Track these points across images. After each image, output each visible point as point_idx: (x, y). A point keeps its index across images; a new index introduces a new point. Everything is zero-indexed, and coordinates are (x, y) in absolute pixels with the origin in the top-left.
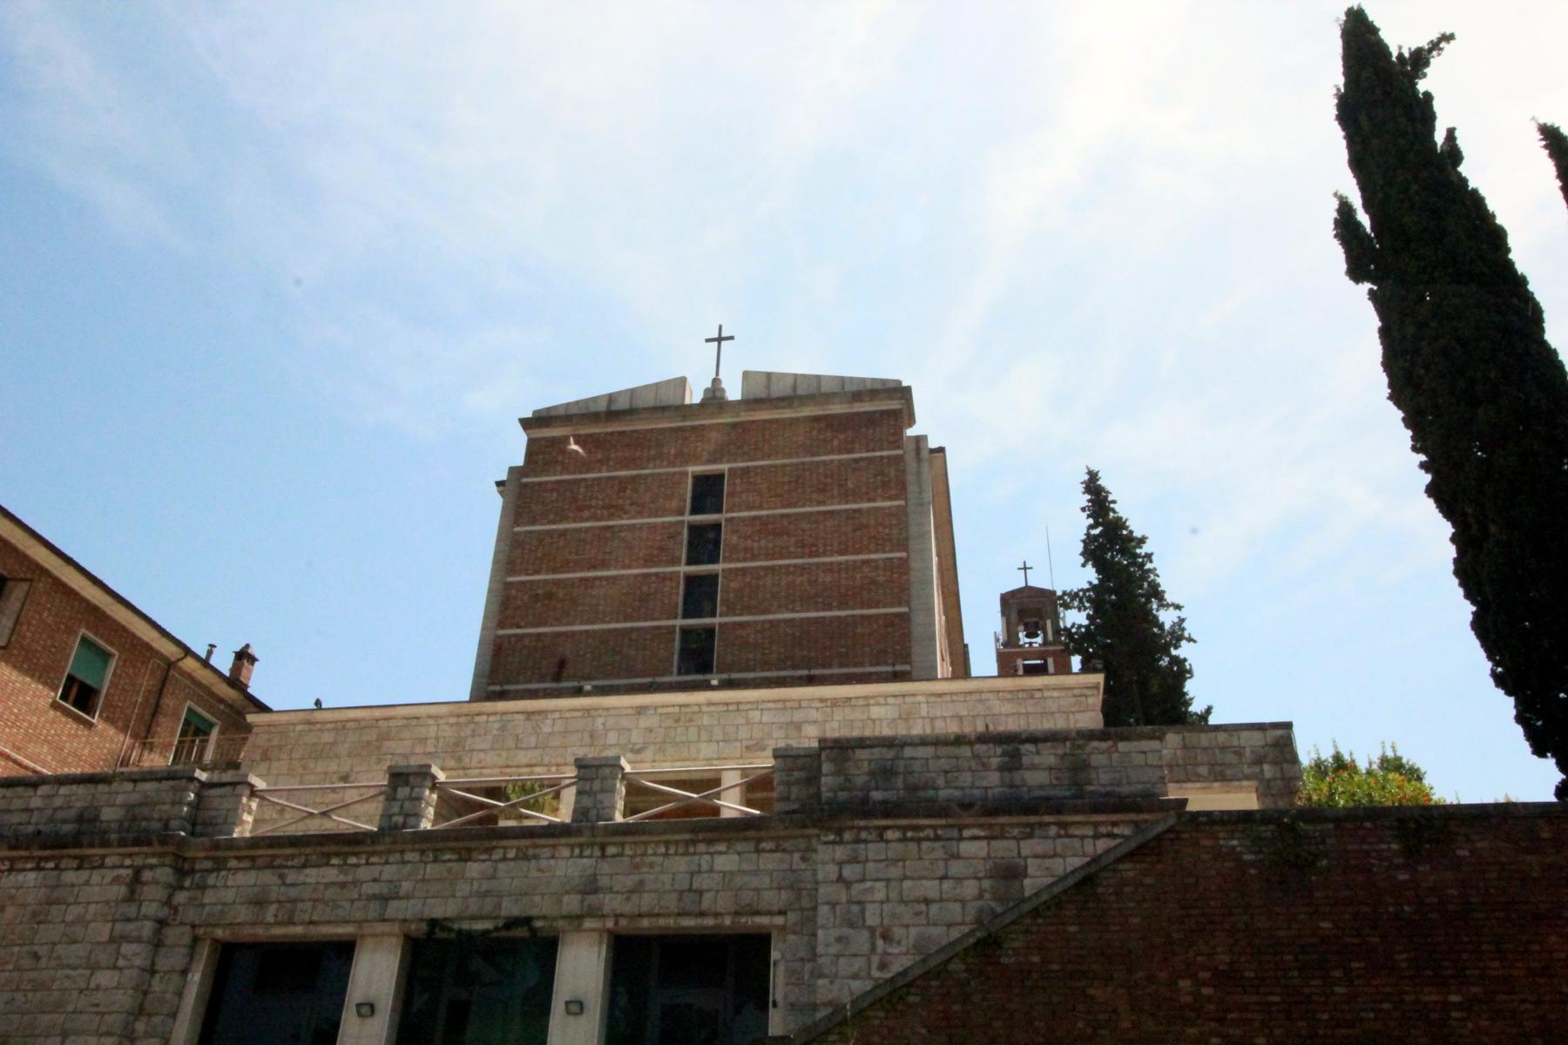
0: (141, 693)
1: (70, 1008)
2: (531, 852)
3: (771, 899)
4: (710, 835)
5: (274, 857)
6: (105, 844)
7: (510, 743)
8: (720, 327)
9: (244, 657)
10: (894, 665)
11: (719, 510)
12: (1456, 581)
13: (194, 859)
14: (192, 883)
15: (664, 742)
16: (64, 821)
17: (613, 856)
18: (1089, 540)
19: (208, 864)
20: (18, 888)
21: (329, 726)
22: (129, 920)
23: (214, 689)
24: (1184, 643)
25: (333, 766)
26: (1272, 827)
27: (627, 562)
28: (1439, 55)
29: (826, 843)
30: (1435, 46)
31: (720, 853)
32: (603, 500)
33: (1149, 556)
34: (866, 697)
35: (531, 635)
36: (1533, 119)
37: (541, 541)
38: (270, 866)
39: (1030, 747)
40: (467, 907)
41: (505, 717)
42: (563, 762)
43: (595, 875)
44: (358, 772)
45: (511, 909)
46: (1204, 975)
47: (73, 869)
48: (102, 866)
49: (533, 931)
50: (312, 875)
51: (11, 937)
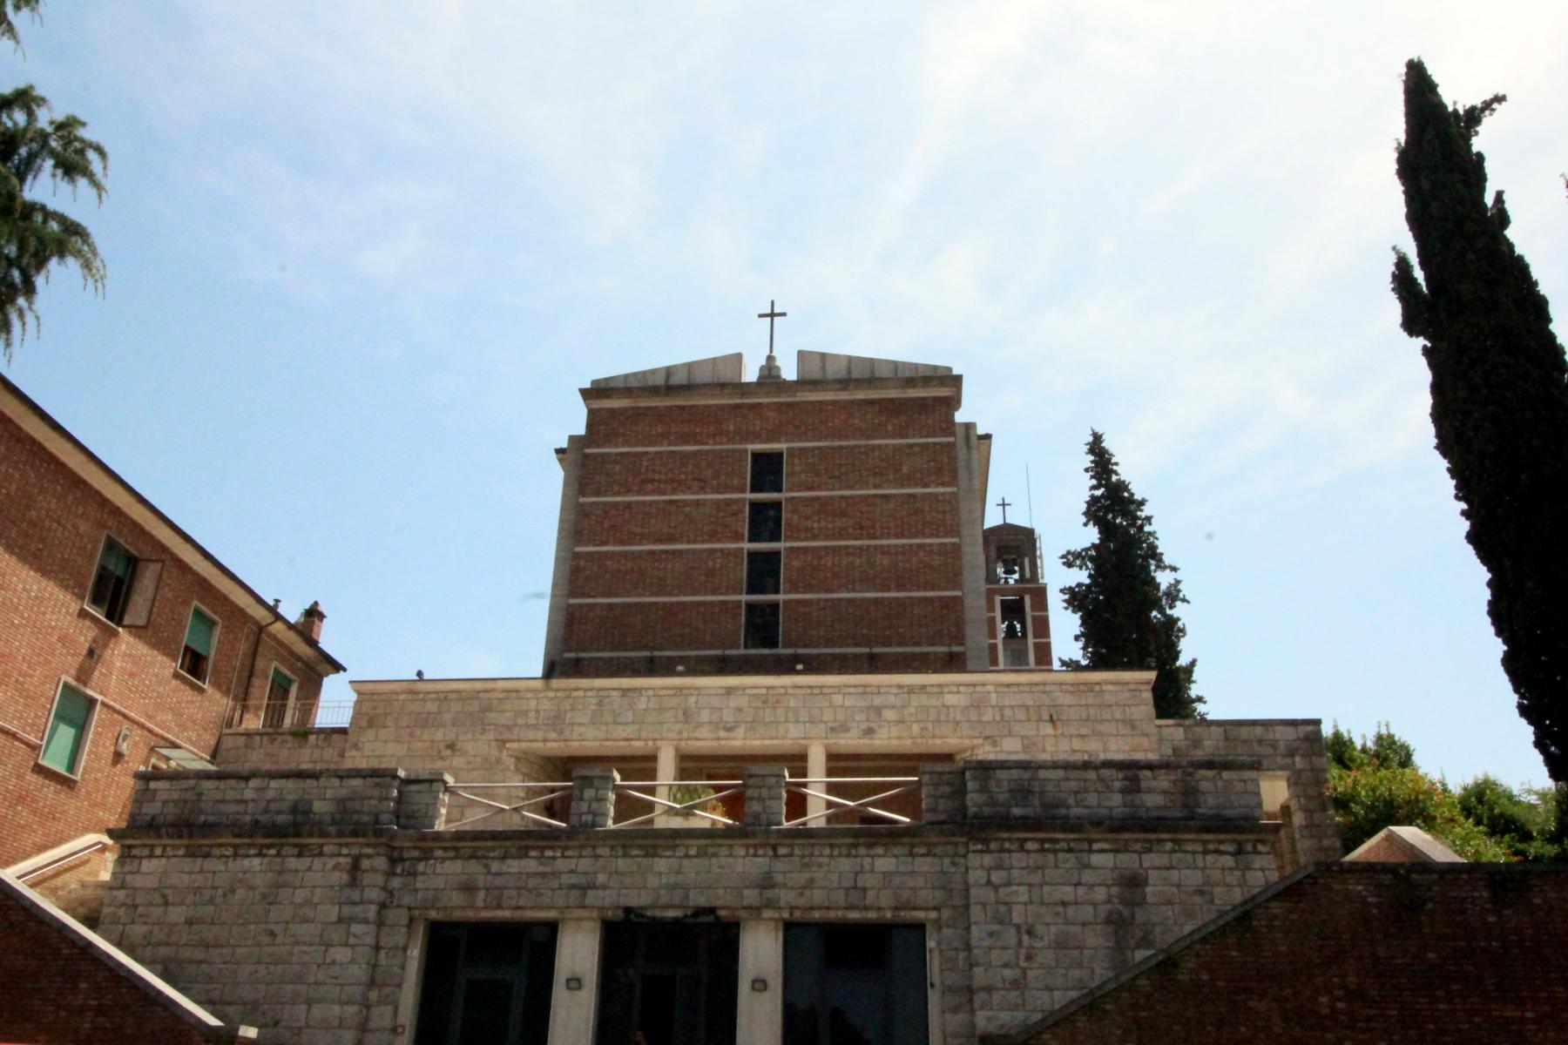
0: (240, 658)
1: (312, 980)
2: (711, 850)
3: (926, 896)
4: (868, 840)
5: (476, 849)
6: (324, 834)
7: (608, 717)
8: (773, 303)
9: (313, 614)
10: (950, 645)
11: (779, 490)
12: (1488, 620)
13: (401, 849)
14: (403, 870)
15: (754, 721)
16: (279, 812)
17: (784, 856)
18: (1093, 501)
19: (416, 854)
20: (245, 873)
21: (432, 696)
22: (353, 903)
23: (294, 648)
24: (1178, 603)
25: (439, 735)
26: (1390, 876)
27: (692, 537)
28: (1491, 115)
29: (974, 851)
30: (1487, 106)
31: (879, 856)
32: (666, 474)
33: (1148, 519)
34: (940, 686)
35: (601, 605)
36: (1562, 175)
37: (606, 513)
38: (473, 857)
39: (1147, 773)
40: (659, 898)
41: (601, 693)
42: (659, 737)
43: (769, 873)
44: (463, 741)
45: (699, 899)
46: (1338, 993)
47: (293, 856)
48: (321, 854)
49: (718, 918)
50: (513, 866)
51: (247, 916)
